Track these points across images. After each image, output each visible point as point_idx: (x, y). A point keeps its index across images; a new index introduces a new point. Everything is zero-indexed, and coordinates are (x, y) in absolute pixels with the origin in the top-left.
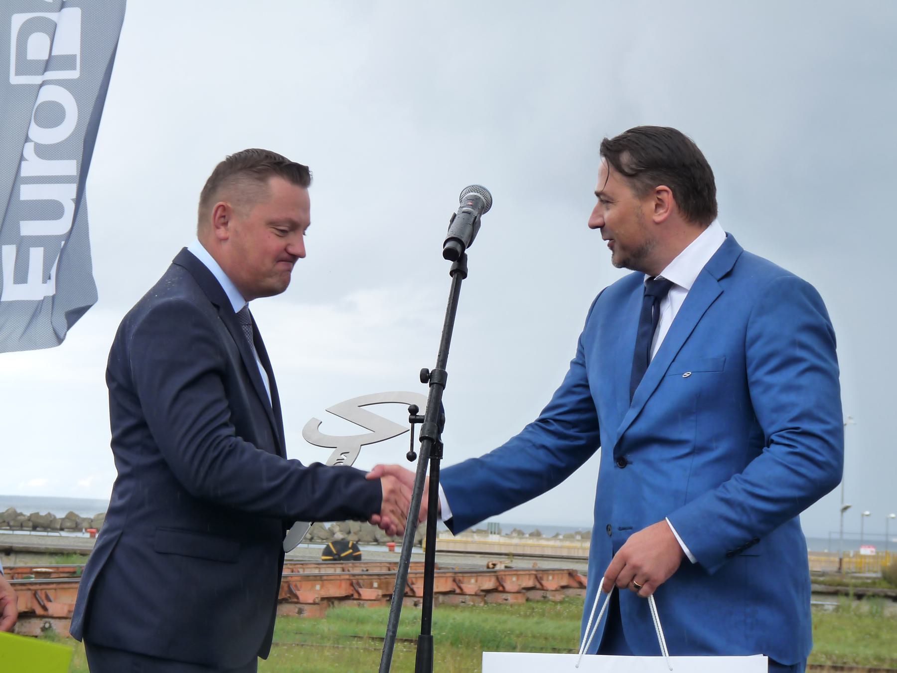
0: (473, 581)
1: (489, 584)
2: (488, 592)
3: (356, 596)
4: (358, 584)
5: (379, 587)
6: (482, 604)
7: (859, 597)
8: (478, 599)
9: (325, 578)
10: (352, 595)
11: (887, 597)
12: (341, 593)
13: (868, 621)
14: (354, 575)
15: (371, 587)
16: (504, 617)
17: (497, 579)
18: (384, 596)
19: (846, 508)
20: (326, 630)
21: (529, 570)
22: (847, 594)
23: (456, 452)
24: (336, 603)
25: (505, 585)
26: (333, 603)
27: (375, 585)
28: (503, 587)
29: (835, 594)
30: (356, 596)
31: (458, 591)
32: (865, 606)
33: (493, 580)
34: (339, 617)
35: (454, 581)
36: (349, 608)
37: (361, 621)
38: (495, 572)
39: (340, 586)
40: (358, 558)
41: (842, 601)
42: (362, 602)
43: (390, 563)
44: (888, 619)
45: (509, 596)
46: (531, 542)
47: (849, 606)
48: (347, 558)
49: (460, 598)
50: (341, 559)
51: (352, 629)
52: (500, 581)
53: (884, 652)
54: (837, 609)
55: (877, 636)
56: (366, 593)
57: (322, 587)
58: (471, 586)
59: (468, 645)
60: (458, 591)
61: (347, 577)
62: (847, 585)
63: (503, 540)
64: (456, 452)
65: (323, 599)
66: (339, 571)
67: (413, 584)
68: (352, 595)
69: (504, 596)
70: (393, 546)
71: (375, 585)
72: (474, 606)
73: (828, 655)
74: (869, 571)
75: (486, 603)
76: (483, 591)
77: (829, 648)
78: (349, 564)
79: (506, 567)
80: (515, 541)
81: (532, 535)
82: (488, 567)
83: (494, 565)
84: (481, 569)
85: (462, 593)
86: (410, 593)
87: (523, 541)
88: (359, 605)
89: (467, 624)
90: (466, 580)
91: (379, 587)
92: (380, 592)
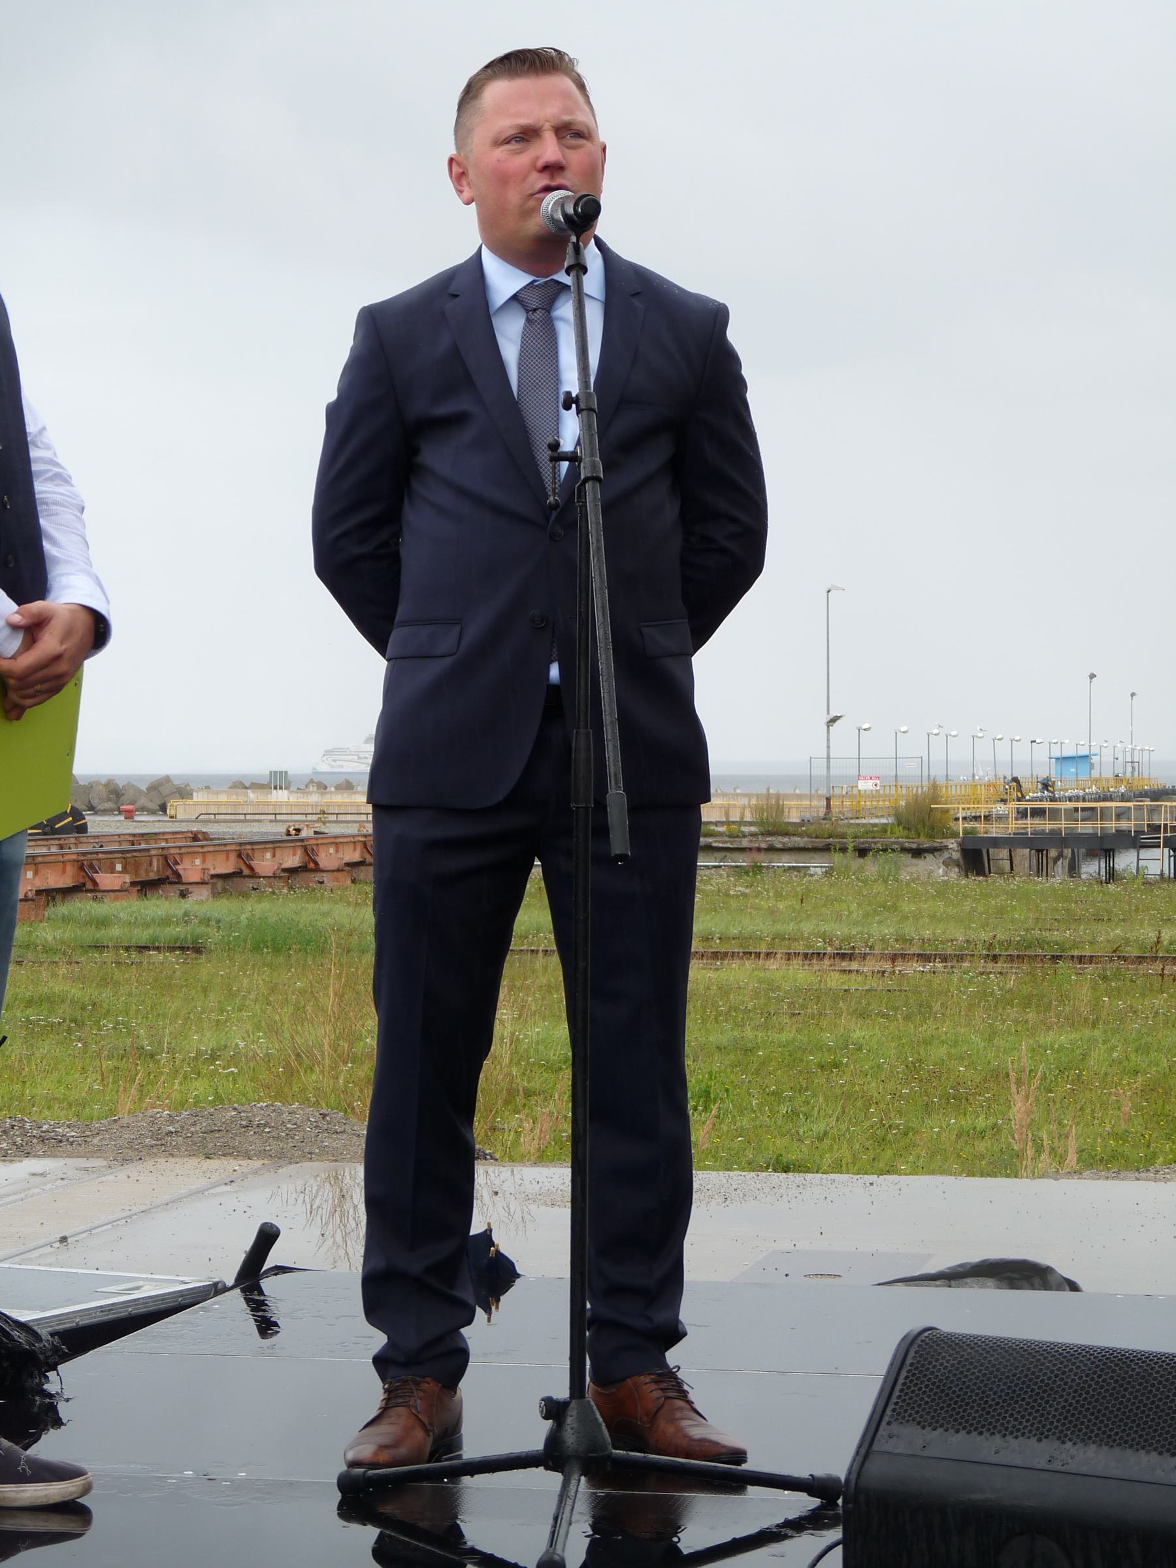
0: (268, 855)
1: (293, 860)
2: (292, 871)
3: (89, 886)
4: (91, 867)
5: (125, 870)
6: (285, 891)
7: (862, 852)
8: (278, 884)
9: (40, 859)
10: (84, 885)
11: (904, 850)
12: (66, 881)
13: (879, 888)
14: (84, 854)
15: (113, 871)
16: (325, 907)
17: (305, 848)
18: (133, 884)
19: (834, 720)
20: (50, 938)
21: (354, 836)
22: (843, 850)
23: (457, 628)
24: (59, 897)
25: (317, 859)
26: (54, 899)
27: (119, 867)
28: (316, 863)
29: (826, 849)
30: (89, 886)
31: (246, 872)
32: (871, 867)
33: (299, 852)
34: (66, 920)
35: (239, 856)
36: (81, 906)
37: (102, 923)
38: (302, 840)
39: (64, 872)
40: (83, 829)
41: (837, 857)
42: (99, 895)
43: (134, 835)
44: (908, 884)
45: (326, 877)
46: (338, 798)
47: (847, 868)
48: (65, 830)
49: (250, 883)
50: (55, 832)
51: (91, 935)
52: (309, 852)
53: (909, 930)
54: (829, 872)
55: (894, 908)
56: (106, 880)
57: (36, 873)
58: (265, 863)
59: (277, 950)
60: (246, 872)
61: (75, 857)
62: (843, 836)
63: (293, 798)
64: (457, 628)
65: (39, 892)
66: (54, 850)
67: (177, 863)
68: (84, 885)
69: (318, 877)
70: (131, 811)
71: (119, 867)
72: (273, 893)
73: (828, 939)
74: (872, 815)
75: (291, 888)
76: (284, 870)
77: (825, 927)
78: (71, 839)
79: (316, 833)
80: (314, 798)
81: (339, 788)
82: (288, 834)
83: (298, 830)
84: (279, 838)
85: (254, 875)
86: (173, 879)
87: (327, 799)
88: (95, 899)
89: (272, 920)
90: (257, 855)
91: (125, 870)
92: (128, 879)
